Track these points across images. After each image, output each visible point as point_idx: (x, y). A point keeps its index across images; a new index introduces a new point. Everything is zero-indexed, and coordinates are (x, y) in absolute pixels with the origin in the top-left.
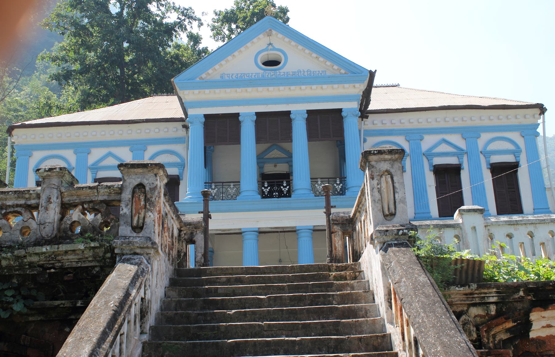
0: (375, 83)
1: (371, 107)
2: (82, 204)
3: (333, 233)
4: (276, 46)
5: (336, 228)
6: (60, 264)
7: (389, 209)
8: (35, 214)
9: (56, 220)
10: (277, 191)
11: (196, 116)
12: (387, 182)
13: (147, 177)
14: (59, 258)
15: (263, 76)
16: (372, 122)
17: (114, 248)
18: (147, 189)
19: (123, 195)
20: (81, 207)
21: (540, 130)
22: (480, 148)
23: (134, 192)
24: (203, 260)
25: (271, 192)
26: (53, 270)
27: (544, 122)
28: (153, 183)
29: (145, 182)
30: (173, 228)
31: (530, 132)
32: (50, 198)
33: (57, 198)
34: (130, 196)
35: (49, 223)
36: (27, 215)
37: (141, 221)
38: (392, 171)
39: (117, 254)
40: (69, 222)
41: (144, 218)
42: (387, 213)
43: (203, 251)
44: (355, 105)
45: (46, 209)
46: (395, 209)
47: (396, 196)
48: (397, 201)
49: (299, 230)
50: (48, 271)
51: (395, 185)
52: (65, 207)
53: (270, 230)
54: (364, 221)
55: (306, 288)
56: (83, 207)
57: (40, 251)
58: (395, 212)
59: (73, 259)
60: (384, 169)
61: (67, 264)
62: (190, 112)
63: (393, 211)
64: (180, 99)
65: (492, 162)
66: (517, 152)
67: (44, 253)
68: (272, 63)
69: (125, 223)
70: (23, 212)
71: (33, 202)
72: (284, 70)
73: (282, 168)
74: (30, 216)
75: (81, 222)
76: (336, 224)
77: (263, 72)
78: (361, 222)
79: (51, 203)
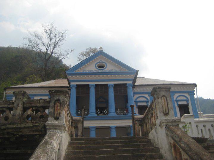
0: (138, 77)
1: (136, 84)
2: (32, 107)
3: (135, 124)
4: (103, 61)
5: (136, 122)
6: (21, 133)
7: (166, 111)
8: (12, 112)
9: (20, 114)
10: (103, 113)
11: (73, 86)
12: (164, 100)
13: (61, 96)
14: (21, 130)
15: (98, 71)
16: (137, 90)
17: (46, 126)
18: (61, 101)
19: (51, 104)
20: (32, 109)
21: (195, 93)
22: (175, 99)
23: (55, 104)
24: (81, 135)
25: (100, 113)
26: (18, 136)
27: (196, 90)
28: (64, 99)
29: (60, 98)
30: (69, 120)
31: (192, 93)
32: (18, 104)
33: (22, 105)
34: (54, 104)
35: (18, 115)
36: (8, 112)
37: (58, 115)
38: (166, 95)
39: (47, 129)
40: (26, 115)
41: (60, 114)
42: (165, 113)
43: (81, 131)
44: (131, 82)
45: (16, 109)
46: (168, 111)
47: (169, 106)
48: (169, 108)
49: (111, 127)
50: (15, 136)
51: (168, 101)
52: (25, 109)
53: (100, 127)
54: (150, 119)
55: (128, 146)
56: (33, 109)
57: (13, 127)
58: (169, 113)
59: (27, 131)
60: (163, 95)
61: (24, 133)
62: (72, 84)
63: (168, 112)
64: (68, 79)
65: (179, 104)
66: (187, 100)
67: (14, 128)
68: (101, 67)
69: (51, 116)
70: (6, 110)
71: (11, 106)
72: (106, 69)
73: (104, 105)
74: (9, 112)
75: (31, 115)
76: (137, 121)
77: (98, 70)
78: (148, 119)
79: (19, 106)
